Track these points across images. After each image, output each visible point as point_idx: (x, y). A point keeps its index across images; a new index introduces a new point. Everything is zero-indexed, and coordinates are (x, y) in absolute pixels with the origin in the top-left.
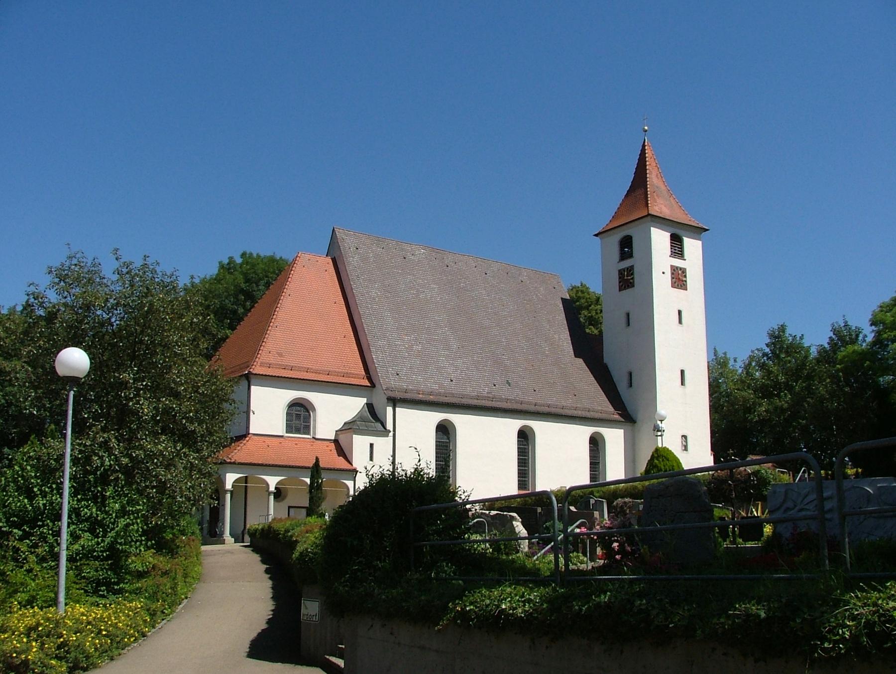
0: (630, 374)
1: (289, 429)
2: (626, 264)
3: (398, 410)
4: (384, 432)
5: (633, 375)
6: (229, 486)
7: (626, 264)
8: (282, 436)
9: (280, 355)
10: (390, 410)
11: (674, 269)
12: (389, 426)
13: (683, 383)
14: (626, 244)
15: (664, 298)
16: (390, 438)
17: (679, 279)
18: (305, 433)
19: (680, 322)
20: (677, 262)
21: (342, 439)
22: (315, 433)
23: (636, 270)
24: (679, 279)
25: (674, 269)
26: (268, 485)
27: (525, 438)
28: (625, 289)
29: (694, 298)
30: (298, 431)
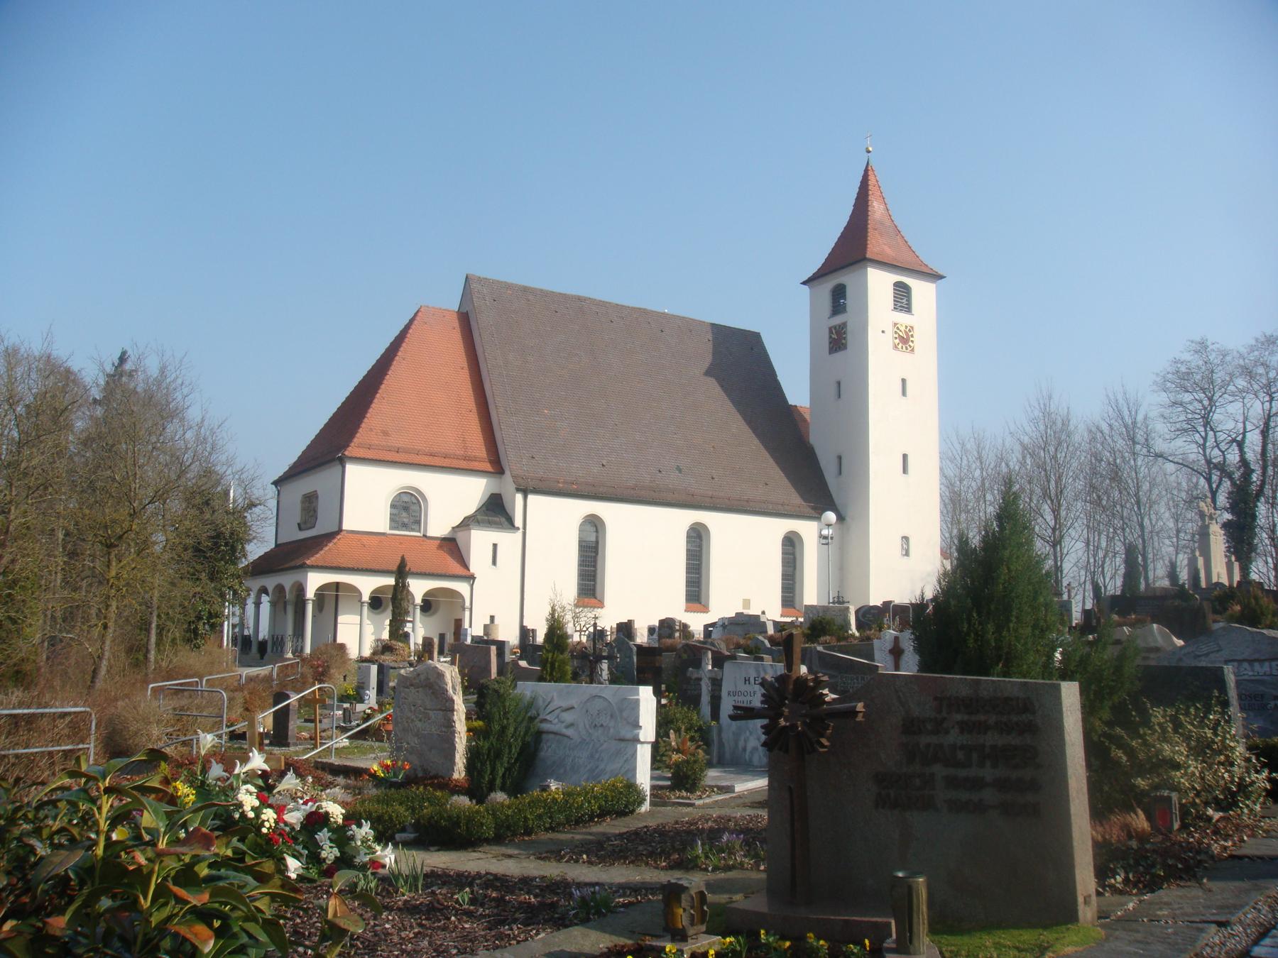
0: (840, 458)
1: (391, 528)
2: (838, 320)
3: (531, 497)
4: (509, 523)
5: (844, 461)
6: (310, 593)
7: (838, 320)
8: (383, 534)
9: (385, 433)
10: (519, 497)
11: (907, 308)
12: (518, 522)
13: (905, 471)
14: (839, 294)
15: (882, 363)
16: (519, 534)
17: (904, 340)
18: (413, 530)
19: (904, 393)
20: (902, 318)
21: (460, 537)
22: (426, 529)
23: (849, 328)
24: (904, 340)
25: (907, 308)
26: (360, 594)
27: (697, 539)
28: (836, 351)
29: (923, 364)
30: (405, 526)
